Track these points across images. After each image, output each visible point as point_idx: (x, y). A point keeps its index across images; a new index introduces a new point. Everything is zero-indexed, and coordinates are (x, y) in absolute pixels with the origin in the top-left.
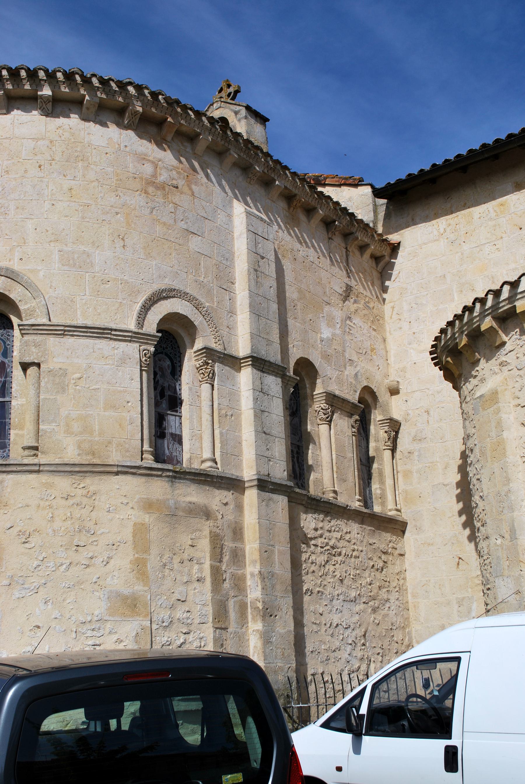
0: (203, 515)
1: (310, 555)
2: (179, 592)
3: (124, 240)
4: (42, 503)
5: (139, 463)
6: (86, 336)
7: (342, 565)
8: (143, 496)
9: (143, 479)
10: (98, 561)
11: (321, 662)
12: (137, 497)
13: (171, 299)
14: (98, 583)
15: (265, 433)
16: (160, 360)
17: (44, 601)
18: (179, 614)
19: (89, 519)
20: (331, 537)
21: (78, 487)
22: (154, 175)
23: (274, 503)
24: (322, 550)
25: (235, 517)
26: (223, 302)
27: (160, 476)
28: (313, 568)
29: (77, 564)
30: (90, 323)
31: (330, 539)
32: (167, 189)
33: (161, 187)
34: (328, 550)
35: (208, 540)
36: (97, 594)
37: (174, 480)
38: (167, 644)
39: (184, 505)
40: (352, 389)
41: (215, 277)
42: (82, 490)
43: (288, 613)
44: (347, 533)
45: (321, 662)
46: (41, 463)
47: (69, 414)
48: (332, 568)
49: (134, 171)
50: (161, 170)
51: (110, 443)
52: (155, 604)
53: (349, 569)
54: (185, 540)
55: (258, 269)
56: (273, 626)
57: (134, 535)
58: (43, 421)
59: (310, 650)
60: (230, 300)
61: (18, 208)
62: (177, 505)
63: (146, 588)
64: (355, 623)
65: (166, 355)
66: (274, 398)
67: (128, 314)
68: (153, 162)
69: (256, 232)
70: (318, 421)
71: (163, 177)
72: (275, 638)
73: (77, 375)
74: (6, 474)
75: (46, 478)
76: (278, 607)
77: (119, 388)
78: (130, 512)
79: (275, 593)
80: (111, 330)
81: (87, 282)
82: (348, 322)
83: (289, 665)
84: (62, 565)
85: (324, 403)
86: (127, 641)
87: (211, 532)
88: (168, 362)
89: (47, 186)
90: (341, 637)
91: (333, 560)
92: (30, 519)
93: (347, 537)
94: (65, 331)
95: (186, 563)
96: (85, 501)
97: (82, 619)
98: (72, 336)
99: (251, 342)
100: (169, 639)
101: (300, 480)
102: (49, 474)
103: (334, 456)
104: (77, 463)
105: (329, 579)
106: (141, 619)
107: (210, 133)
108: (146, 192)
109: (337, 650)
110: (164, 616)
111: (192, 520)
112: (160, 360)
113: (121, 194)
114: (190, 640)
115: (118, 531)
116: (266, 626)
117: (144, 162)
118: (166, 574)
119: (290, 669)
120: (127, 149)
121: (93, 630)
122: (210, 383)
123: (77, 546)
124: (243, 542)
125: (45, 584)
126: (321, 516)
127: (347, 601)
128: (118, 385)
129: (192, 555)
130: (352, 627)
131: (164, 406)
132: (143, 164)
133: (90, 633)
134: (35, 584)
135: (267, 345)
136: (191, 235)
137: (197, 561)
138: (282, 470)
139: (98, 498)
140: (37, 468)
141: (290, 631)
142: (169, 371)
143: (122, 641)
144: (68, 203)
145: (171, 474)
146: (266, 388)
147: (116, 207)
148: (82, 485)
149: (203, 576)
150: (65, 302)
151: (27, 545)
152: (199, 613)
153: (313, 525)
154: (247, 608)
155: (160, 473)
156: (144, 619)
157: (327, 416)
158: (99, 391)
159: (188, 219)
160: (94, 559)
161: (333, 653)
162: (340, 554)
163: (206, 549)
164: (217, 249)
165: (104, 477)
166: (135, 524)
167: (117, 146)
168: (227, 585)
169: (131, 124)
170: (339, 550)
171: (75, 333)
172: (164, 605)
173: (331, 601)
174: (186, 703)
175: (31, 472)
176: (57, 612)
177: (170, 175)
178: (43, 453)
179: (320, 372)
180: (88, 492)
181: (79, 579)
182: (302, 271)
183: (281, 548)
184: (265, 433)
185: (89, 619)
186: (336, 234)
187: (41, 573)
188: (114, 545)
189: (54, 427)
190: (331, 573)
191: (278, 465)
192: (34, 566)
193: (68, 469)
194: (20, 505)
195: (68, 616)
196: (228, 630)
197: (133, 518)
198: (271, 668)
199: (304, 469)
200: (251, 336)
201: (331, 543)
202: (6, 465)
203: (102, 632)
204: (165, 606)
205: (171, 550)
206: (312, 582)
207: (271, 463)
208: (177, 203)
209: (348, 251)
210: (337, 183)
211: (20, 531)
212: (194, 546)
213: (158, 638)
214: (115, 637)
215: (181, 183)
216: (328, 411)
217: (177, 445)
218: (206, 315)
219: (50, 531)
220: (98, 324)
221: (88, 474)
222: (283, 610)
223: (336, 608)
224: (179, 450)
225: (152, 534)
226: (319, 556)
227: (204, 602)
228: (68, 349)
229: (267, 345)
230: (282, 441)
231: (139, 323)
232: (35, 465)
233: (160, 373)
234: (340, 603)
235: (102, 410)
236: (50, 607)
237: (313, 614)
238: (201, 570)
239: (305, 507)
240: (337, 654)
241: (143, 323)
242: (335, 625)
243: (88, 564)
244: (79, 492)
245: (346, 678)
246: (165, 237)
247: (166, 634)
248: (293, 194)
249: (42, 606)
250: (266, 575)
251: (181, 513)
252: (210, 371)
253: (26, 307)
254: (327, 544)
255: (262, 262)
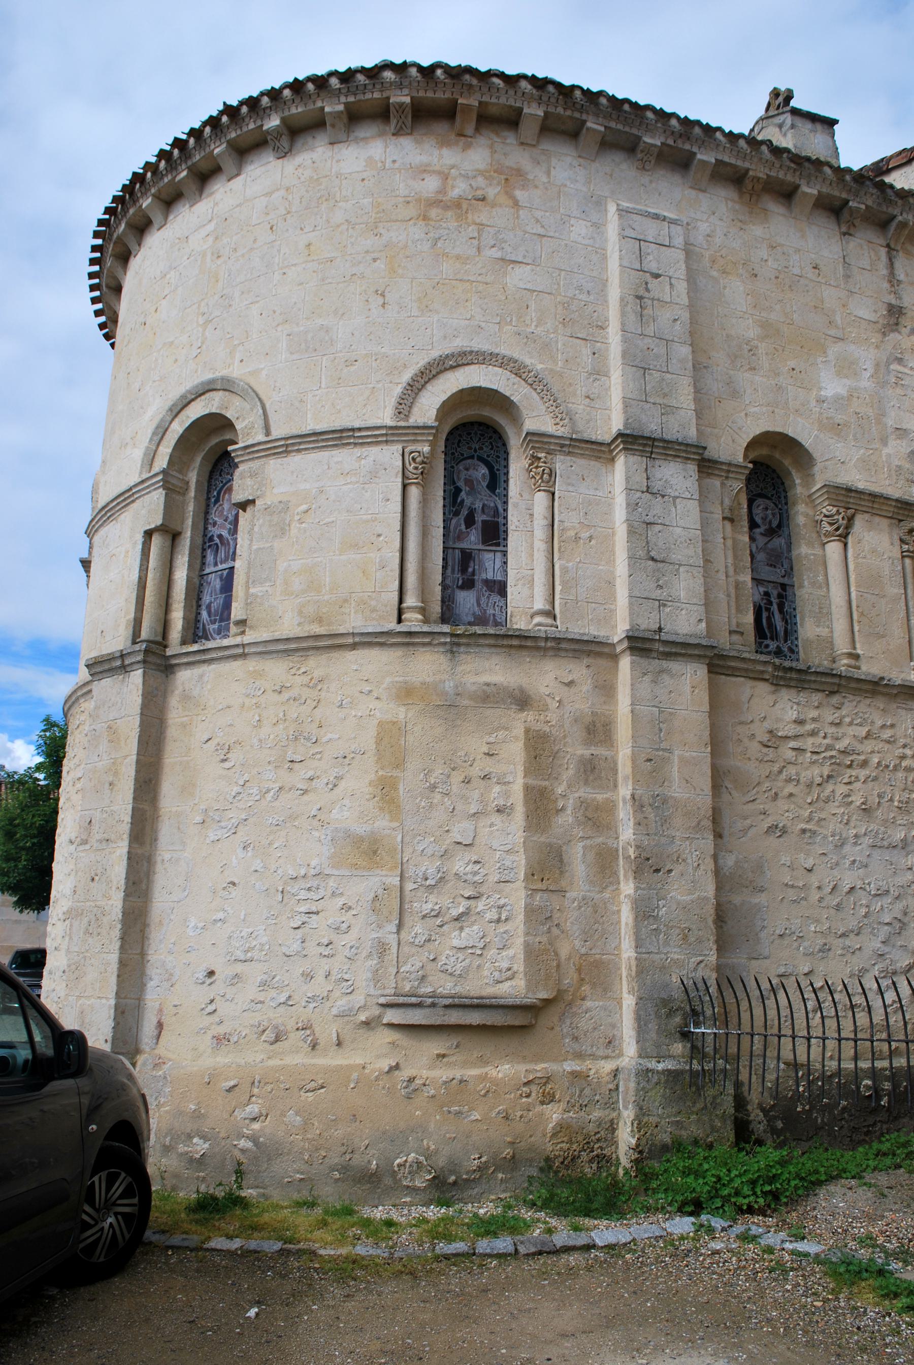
0: (511, 704)
1: (784, 767)
2: (461, 830)
3: (384, 296)
4: (247, 702)
5: (392, 625)
6: (318, 448)
7: (871, 784)
8: (397, 679)
9: (399, 652)
10: (319, 784)
11: (805, 955)
12: (388, 680)
13: (467, 368)
14: (318, 818)
15: (653, 559)
16: (467, 469)
17: (242, 846)
18: (460, 864)
19: (310, 719)
20: (840, 735)
21: (298, 673)
22: (442, 191)
23: (672, 676)
24: (815, 757)
25: (593, 704)
26: (578, 360)
27: (429, 644)
28: (790, 788)
29: (290, 789)
30: (320, 427)
31: (837, 739)
32: (465, 206)
33: (457, 204)
34: (832, 757)
35: (521, 744)
36: (316, 834)
37: (455, 649)
38: (432, 914)
39: (474, 688)
40: (901, 477)
41: (560, 323)
42: (302, 677)
43: (702, 867)
44: (883, 726)
45: (805, 955)
46: (245, 642)
47: (290, 566)
48: (842, 789)
49: (406, 193)
50: (455, 180)
51: (346, 601)
52: (411, 850)
53: (888, 791)
54: (476, 745)
55: (646, 295)
56: (661, 889)
57: (379, 740)
58: (254, 581)
59: (778, 932)
60: (594, 354)
61: (243, 293)
62: (460, 689)
63: (395, 824)
64: (902, 887)
65: (481, 459)
66: (678, 500)
67: (385, 402)
68: (439, 173)
69: (641, 237)
70: (823, 538)
71: (459, 189)
72: (664, 909)
73: (304, 507)
74: (206, 665)
75: (254, 664)
76: (676, 855)
77: (365, 517)
78: (373, 704)
79: (673, 833)
80: (353, 430)
81: (324, 368)
82: (894, 366)
83: (701, 958)
84: (268, 791)
85: (828, 505)
86: (359, 908)
87: (527, 731)
88: (483, 470)
89: (279, 251)
90: (863, 911)
91: (847, 775)
92: (231, 725)
93: (886, 734)
94: (287, 446)
95: (476, 782)
96: (306, 692)
97: (292, 872)
98: (299, 451)
99: (625, 412)
100: (437, 907)
101: (786, 641)
102: (257, 658)
103: (853, 595)
104: (291, 636)
105: (833, 808)
106: (384, 873)
107: (539, 104)
108: (425, 218)
109: (852, 935)
110: (427, 869)
111: (489, 712)
112: (467, 469)
113: (382, 231)
114: (478, 910)
115: (353, 736)
116: (641, 889)
117: (425, 175)
118: (435, 801)
119: (702, 965)
120: (397, 165)
121: (309, 889)
122: (544, 490)
123: (292, 761)
124: (613, 746)
125: (245, 820)
126: (816, 698)
127: (880, 847)
128: (362, 512)
129: (488, 769)
130: (894, 892)
131: (473, 538)
132: (423, 180)
133: (303, 895)
134: (233, 821)
135: (662, 414)
136: (512, 266)
137: (498, 779)
138: (693, 620)
139: (325, 687)
140: (240, 651)
141: (706, 899)
142: (485, 484)
143: (350, 908)
144: (304, 265)
145: (448, 640)
146: (657, 486)
147: (373, 252)
148: (303, 670)
149: (509, 804)
150: (292, 405)
151: (227, 765)
152: (498, 865)
153: (792, 714)
154: (617, 859)
155: (427, 640)
156: (389, 873)
157: (835, 526)
158: (333, 525)
159: (506, 242)
160: (315, 780)
161: (840, 940)
162: (864, 764)
163: (518, 759)
164: (565, 279)
165: (336, 654)
166: (380, 724)
167: (380, 165)
168: (566, 819)
169: (401, 127)
170: (862, 757)
171: (302, 447)
172: (429, 851)
173: (836, 846)
174: (460, 1013)
175: (235, 657)
176: (259, 861)
177: (470, 185)
178: (251, 627)
179: (816, 455)
180: (311, 679)
181: (291, 811)
182: (772, 292)
183: (687, 754)
184: (653, 559)
185: (303, 872)
186: (857, 224)
187: (241, 805)
188: (345, 757)
189: (268, 589)
190: (838, 798)
191: (684, 612)
192: (233, 794)
193: (281, 647)
194: (220, 707)
195: (273, 868)
196: (568, 895)
197: (378, 715)
198: (653, 962)
199: (795, 624)
200: (624, 402)
201: (841, 745)
202: (204, 651)
203: (321, 893)
204: (432, 852)
205: (448, 762)
206: (787, 814)
207: (668, 610)
208: (484, 222)
209: (894, 250)
210: (905, 160)
211: (219, 744)
212: (492, 755)
213: (415, 904)
214: (340, 901)
215: (492, 192)
216: (836, 517)
217: (495, 598)
218: (536, 382)
219: (255, 741)
220: (337, 425)
221: (310, 653)
222: (689, 861)
223: (852, 859)
224: (501, 604)
225: (410, 738)
226: (807, 769)
227: (509, 847)
228: (292, 472)
229: (662, 414)
230: (694, 572)
231: (400, 413)
232: (237, 646)
233: (468, 489)
234: (862, 851)
235: (337, 552)
236: (250, 854)
237: (787, 869)
238: (507, 795)
239: (772, 684)
240: (853, 942)
241: (409, 412)
242: (846, 889)
243: (305, 788)
244: (299, 680)
245: (872, 985)
246: (458, 277)
247: (432, 898)
248: (743, 171)
249: (240, 853)
250: (646, 800)
251: (466, 702)
252: (544, 470)
253: (243, 425)
254: (829, 748)
255: (653, 284)
